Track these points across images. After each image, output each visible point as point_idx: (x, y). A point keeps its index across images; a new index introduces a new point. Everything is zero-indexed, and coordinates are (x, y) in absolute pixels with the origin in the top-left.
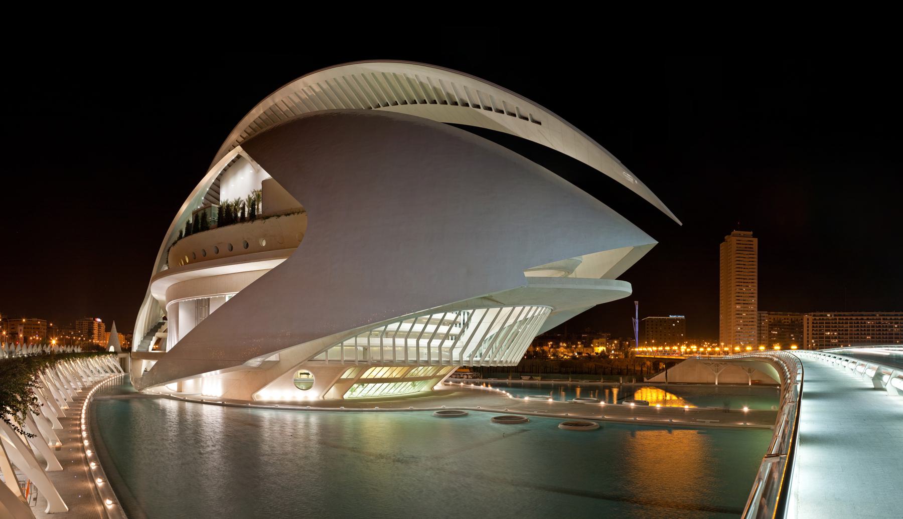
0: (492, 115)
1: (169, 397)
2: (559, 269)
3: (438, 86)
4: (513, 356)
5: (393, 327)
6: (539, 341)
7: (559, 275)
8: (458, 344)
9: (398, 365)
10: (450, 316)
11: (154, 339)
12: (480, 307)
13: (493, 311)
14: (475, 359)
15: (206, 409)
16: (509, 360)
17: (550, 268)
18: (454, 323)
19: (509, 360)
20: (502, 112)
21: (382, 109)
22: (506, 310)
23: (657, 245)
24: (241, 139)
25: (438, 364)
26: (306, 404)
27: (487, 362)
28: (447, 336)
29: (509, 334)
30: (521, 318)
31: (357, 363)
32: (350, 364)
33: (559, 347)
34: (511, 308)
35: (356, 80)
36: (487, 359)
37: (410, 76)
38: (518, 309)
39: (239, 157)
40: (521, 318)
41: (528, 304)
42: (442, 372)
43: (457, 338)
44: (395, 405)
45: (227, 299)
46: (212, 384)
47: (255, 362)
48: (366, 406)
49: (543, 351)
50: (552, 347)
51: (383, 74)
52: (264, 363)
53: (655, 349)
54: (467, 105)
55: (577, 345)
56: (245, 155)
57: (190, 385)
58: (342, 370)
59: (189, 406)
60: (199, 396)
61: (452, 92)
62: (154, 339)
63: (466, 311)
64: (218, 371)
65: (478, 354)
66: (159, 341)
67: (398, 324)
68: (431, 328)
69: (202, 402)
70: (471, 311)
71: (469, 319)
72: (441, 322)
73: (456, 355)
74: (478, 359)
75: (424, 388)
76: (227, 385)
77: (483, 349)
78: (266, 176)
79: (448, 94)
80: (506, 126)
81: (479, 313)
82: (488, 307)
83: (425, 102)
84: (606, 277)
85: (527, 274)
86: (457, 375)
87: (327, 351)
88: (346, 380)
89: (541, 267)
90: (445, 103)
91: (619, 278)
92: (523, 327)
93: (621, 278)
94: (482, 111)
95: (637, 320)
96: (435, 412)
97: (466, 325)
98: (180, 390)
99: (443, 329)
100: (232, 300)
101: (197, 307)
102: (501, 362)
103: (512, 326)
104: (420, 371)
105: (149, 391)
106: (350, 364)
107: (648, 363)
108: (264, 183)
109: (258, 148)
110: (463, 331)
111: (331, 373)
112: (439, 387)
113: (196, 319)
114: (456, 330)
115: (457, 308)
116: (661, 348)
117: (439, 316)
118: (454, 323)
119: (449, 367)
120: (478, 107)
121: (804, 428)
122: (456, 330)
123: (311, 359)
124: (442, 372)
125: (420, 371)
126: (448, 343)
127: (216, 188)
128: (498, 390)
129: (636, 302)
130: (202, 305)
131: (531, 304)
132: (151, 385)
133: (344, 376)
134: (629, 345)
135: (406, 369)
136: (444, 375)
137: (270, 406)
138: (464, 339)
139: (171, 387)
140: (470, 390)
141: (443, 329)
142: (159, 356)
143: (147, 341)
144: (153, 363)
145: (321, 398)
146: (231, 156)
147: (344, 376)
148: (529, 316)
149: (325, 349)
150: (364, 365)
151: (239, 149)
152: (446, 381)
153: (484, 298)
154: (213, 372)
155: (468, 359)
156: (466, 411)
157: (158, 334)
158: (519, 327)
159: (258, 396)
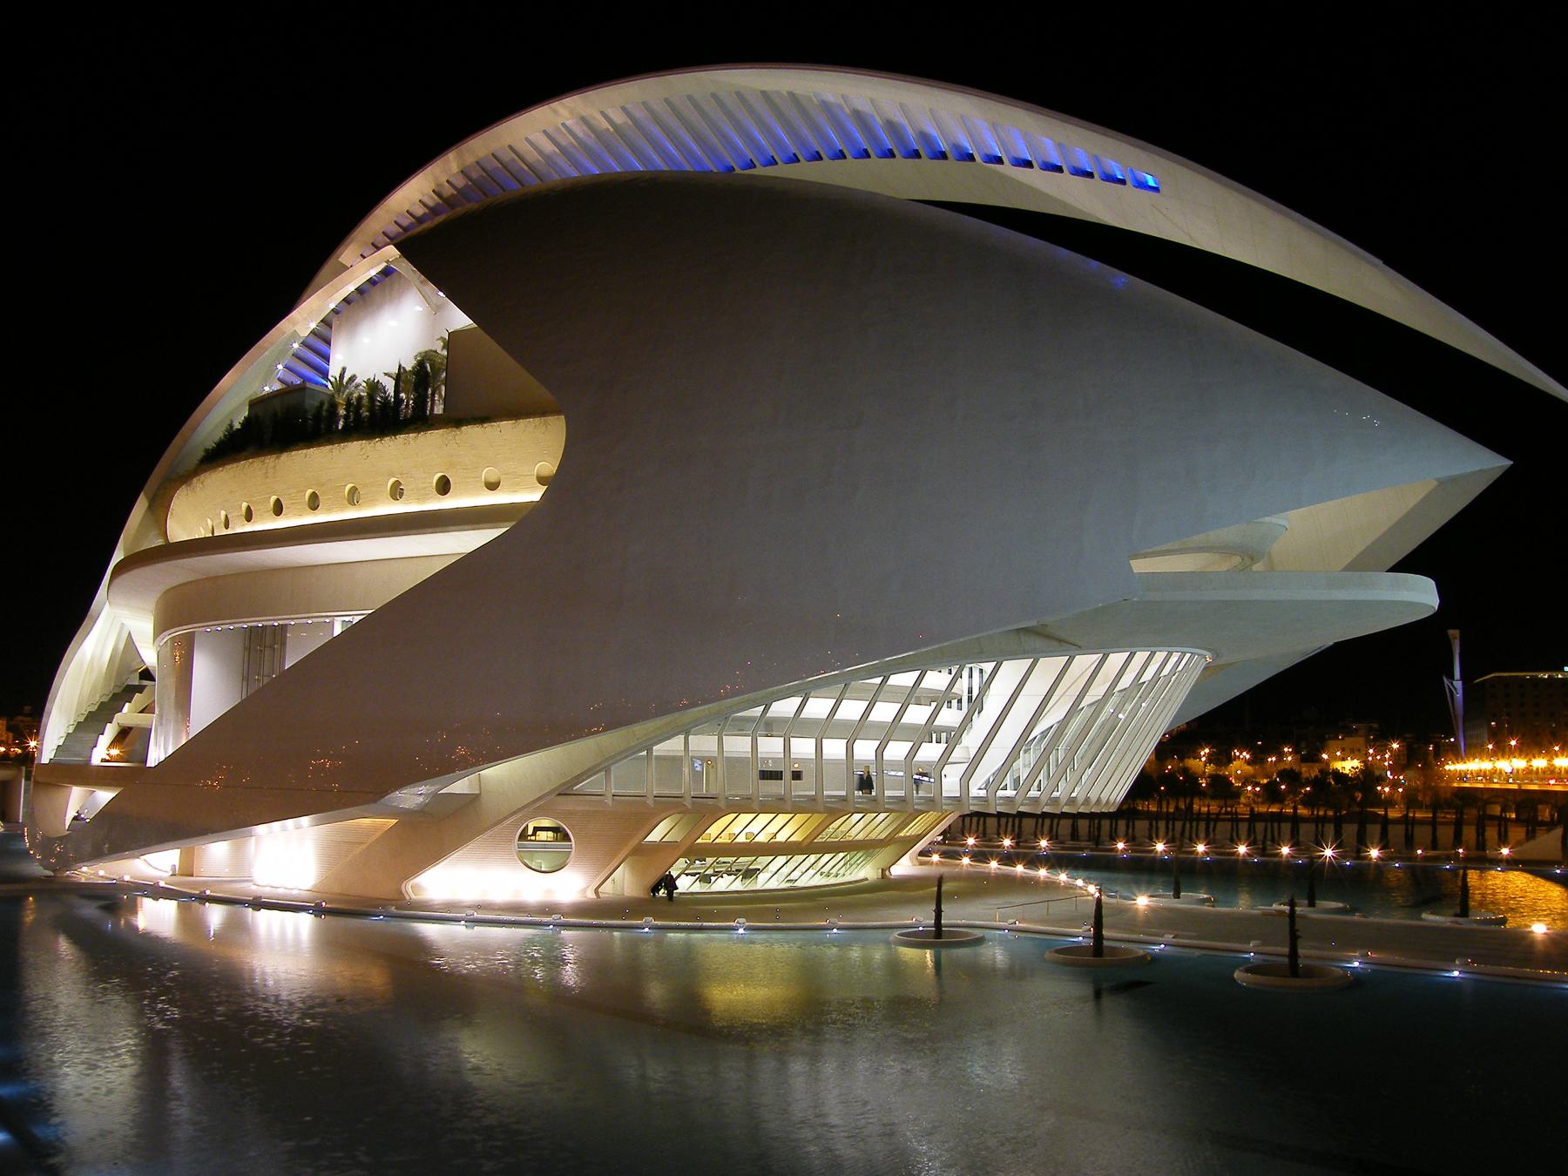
0: (1034, 178)
1: (157, 892)
2: (1224, 550)
3: (899, 118)
4: (1108, 785)
5: (784, 708)
6: (1176, 743)
7: (1224, 567)
8: (957, 754)
9: (795, 810)
10: (936, 680)
11: (110, 731)
12: (1014, 655)
13: (1049, 666)
14: (1000, 793)
15: (265, 921)
16: (1093, 796)
17: (1200, 549)
18: (944, 698)
19: (1093, 796)
20: (1059, 169)
21: (759, 171)
22: (1084, 662)
23: (1507, 474)
24: (395, 229)
25: (904, 809)
26: (548, 909)
27: (1036, 800)
28: (928, 732)
29: (1089, 730)
30: (1126, 681)
31: (688, 803)
32: (668, 805)
33: (1230, 760)
34: (1096, 657)
35: (696, 106)
36: (1033, 793)
37: (830, 98)
38: (1116, 659)
39: (387, 272)
40: (1126, 681)
41: (1144, 645)
42: (911, 830)
43: (953, 737)
44: (777, 914)
45: (338, 630)
46: (287, 855)
47: (411, 797)
48: (711, 916)
49: (1185, 771)
50: (1209, 761)
51: (764, 93)
52: (435, 795)
53: (1519, 763)
54: (971, 158)
55: (1281, 755)
56: (406, 268)
57: (216, 856)
58: (648, 819)
59: (215, 916)
60: (252, 889)
61: (933, 131)
62: (110, 731)
63: (976, 667)
64: (305, 820)
65: (1008, 781)
66: (124, 734)
67: (797, 701)
68: (884, 712)
69: (258, 904)
70: (988, 667)
71: (986, 686)
72: (913, 696)
73: (951, 784)
74: (1010, 793)
75: (866, 871)
76: (333, 854)
77: (1022, 768)
78: (460, 320)
79: (924, 137)
80: (1070, 200)
81: (1012, 670)
82: (1035, 655)
83: (866, 154)
84: (1361, 564)
85: (1140, 566)
86: (952, 836)
87: (607, 771)
88: (660, 846)
89: (1169, 546)
90: (916, 154)
91: (1397, 568)
92: (1129, 707)
93: (1408, 564)
94: (1007, 169)
95: (1458, 684)
96: (896, 934)
97: (976, 704)
98: (187, 869)
99: (917, 715)
100: (351, 631)
101: (248, 649)
102: (1072, 801)
103: (1100, 704)
104: (856, 826)
105: (92, 872)
106: (668, 805)
107: (33, 744)
108: (454, 340)
109: (435, 252)
110: (967, 721)
111: (615, 828)
112: (904, 867)
113: (246, 678)
114: (949, 717)
115: (955, 656)
116: (1540, 763)
117: (905, 679)
118: (944, 698)
119: (932, 816)
120: (999, 160)
121: (160, 542)
122: (949, 717)
123: (565, 791)
124: (911, 830)
125: (856, 826)
126: (930, 752)
127: (320, 343)
128: (1063, 877)
129: (1454, 633)
130: (260, 645)
131: (1152, 645)
132: (97, 854)
133: (655, 836)
134: (1437, 754)
135: (817, 819)
136: (919, 837)
137: (445, 914)
138: (971, 741)
139: (159, 864)
140: (986, 877)
141: (917, 715)
142: (130, 774)
143: (90, 736)
144: (104, 796)
145: (591, 895)
146: (368, 270)
147: (655, 836)
148: (1147, 676)
149: (602, 766)
150: (706, 810)
151: (391, 251)
152: (924, 853)
153: (1026, 630)
154: (290, 822)
155: (983, 793)
156: (979, 933)
157: (128, 714)
158: (1119, 708)
159: (416, 888)
